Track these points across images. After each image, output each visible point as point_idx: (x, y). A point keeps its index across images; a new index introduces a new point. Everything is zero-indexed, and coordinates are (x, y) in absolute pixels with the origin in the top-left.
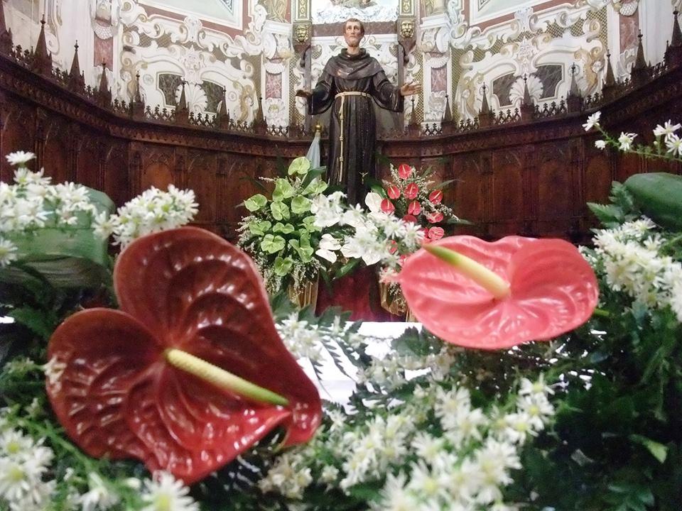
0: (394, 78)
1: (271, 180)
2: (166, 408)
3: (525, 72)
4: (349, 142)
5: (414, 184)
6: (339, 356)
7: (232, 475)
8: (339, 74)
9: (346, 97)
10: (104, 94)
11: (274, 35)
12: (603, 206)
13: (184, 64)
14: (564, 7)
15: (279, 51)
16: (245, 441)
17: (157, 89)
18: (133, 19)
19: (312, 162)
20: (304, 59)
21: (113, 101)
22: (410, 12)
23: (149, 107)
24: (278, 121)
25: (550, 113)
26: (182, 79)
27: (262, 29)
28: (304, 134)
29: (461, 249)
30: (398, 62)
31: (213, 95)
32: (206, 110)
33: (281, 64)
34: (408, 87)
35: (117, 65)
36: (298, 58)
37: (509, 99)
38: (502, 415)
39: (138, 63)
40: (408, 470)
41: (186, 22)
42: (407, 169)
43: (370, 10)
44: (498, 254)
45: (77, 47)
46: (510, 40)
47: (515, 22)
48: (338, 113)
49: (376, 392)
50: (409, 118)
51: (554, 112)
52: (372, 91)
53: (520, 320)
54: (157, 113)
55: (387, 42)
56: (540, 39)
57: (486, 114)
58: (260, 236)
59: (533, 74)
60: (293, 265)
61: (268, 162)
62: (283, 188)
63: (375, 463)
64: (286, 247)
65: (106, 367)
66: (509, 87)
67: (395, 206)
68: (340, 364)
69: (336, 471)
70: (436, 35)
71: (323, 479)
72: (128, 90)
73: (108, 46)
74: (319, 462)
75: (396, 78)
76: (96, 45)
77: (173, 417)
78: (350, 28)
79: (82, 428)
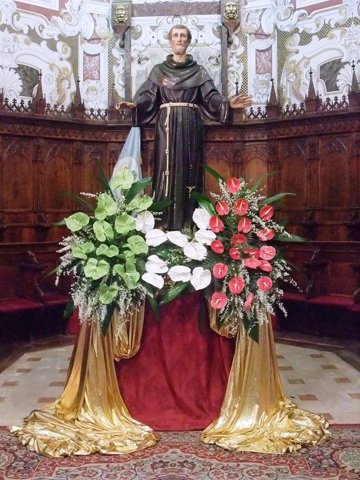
0: (217, 60)
1: (93, 195)
8: (165, 84)
9: (172, 108)
11: (92, 14)
24: (97, 103)
27: (79, 8)
31: (28, 79)
32: (21, 94)
33: (99, 45)
36: (117, 38)
37: (336, 84)
46: (337, 25)
52: (199, 100)
57: (312, 100)
58: (83, 259)
60: (119, 291)
61: (86, 146)
64: (111, 272)
66: (336, 72)
70: (261, 16)
78: (176, 35)
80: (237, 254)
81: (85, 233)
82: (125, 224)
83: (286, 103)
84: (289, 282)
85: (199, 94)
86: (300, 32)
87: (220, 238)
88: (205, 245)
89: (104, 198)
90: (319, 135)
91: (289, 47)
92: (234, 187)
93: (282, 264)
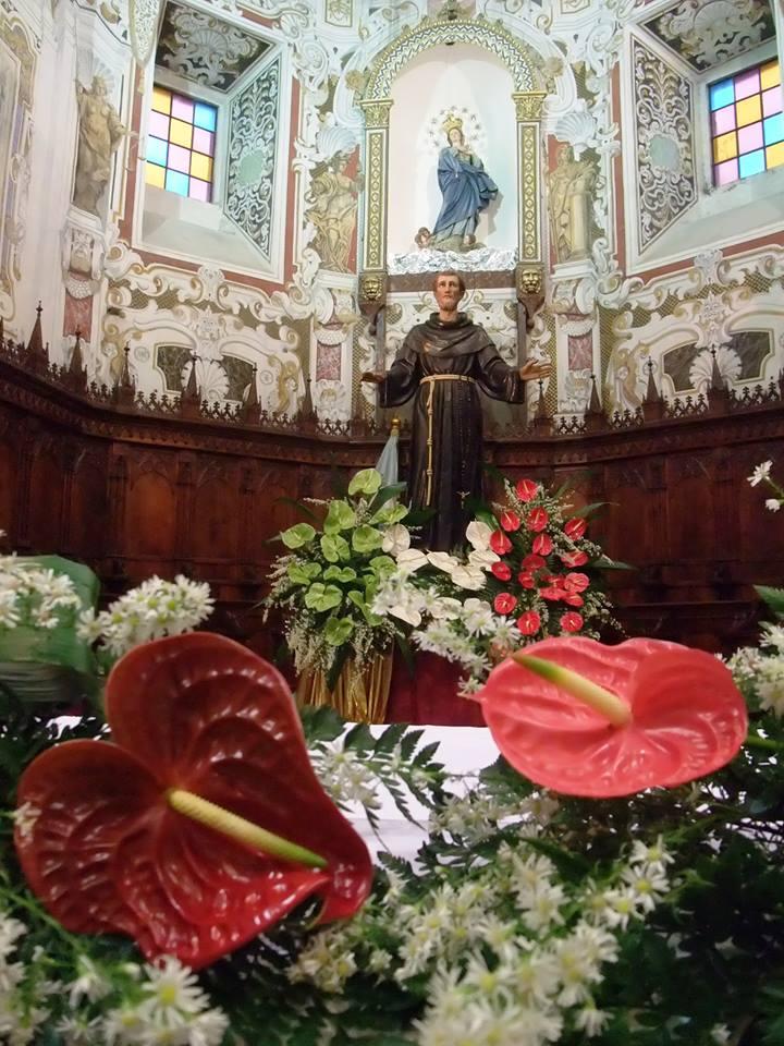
0: (511, 350)
1: (323, 502)
2: (166, 868)
3: (713, 342)
4: (440, 448)
5: (541, 509)
6: (403, 795)
7: (251, 958)
8: (427, 350)
9: (437, 381)
10: (76, 374)
11: (330, 290)
12: (777, 590)
13: (196, 331)
14: (770, 250)
15: (337, 313)
16: (267, 915)
17: (154, 367)
18: (123, 269)
19: (384, 477)
20: (375, 323)
21: (89, 384)
22: (536, 257)
23: (141, 393)
24: (335, 413)
25: (753, 401)
26: (192, 353)
27: (313, 281)
28: (373, 431)
29: (568, 656)
30: (517, 327)
31: (236, 376)
32: (226, 397)
33: (340, 332)
34: (530, 367)
35: (96, 334)
38: (601, 890)
39: (127, 331)
40: (463, 963)
41: (200, 273)
42: (531, 487)
43: (475, 255)
44: (619, 662)
45: (40, 310)
46: (688, 297)
47: (695, 271)
48: (424, 405)
49: (455, 844)
50: (535, 408)
51: (760, 400)
52: (476, 372)
53: (644, 756)
54: (153, 401)
55: (500, 300)
56: (734, 294)
57: (654, 403)
58: (304, 585)
59: (725, 344)
60: (354, 629)
61: (318, 473)
62: (340, 514)
63: (441, 948)
64: (343, 601)
65: (90, 813)
67: (511, 541)
68: (404, 805)
69: (390, 957)
70: (575, 289)
71: (372, 967)
72: (111, 370)
73: (86, 308)
74: (367, 944)
75: (515, 351)
76: (67, 303)
77: (175, 880)
78: (443, 284)
79: (57, 892)
80: (530, 581)
81: (309, 554)
82: (367, 541)
83: (615, 410)
84: (609, 623)
85: (476, 363)
86: (633, 308)
87: (506, 562)
88: (483, 570)
89: (337, 506)
90: (664, 454)
91: (617, 330)
92: (528, 492)
93: (597, 597)
